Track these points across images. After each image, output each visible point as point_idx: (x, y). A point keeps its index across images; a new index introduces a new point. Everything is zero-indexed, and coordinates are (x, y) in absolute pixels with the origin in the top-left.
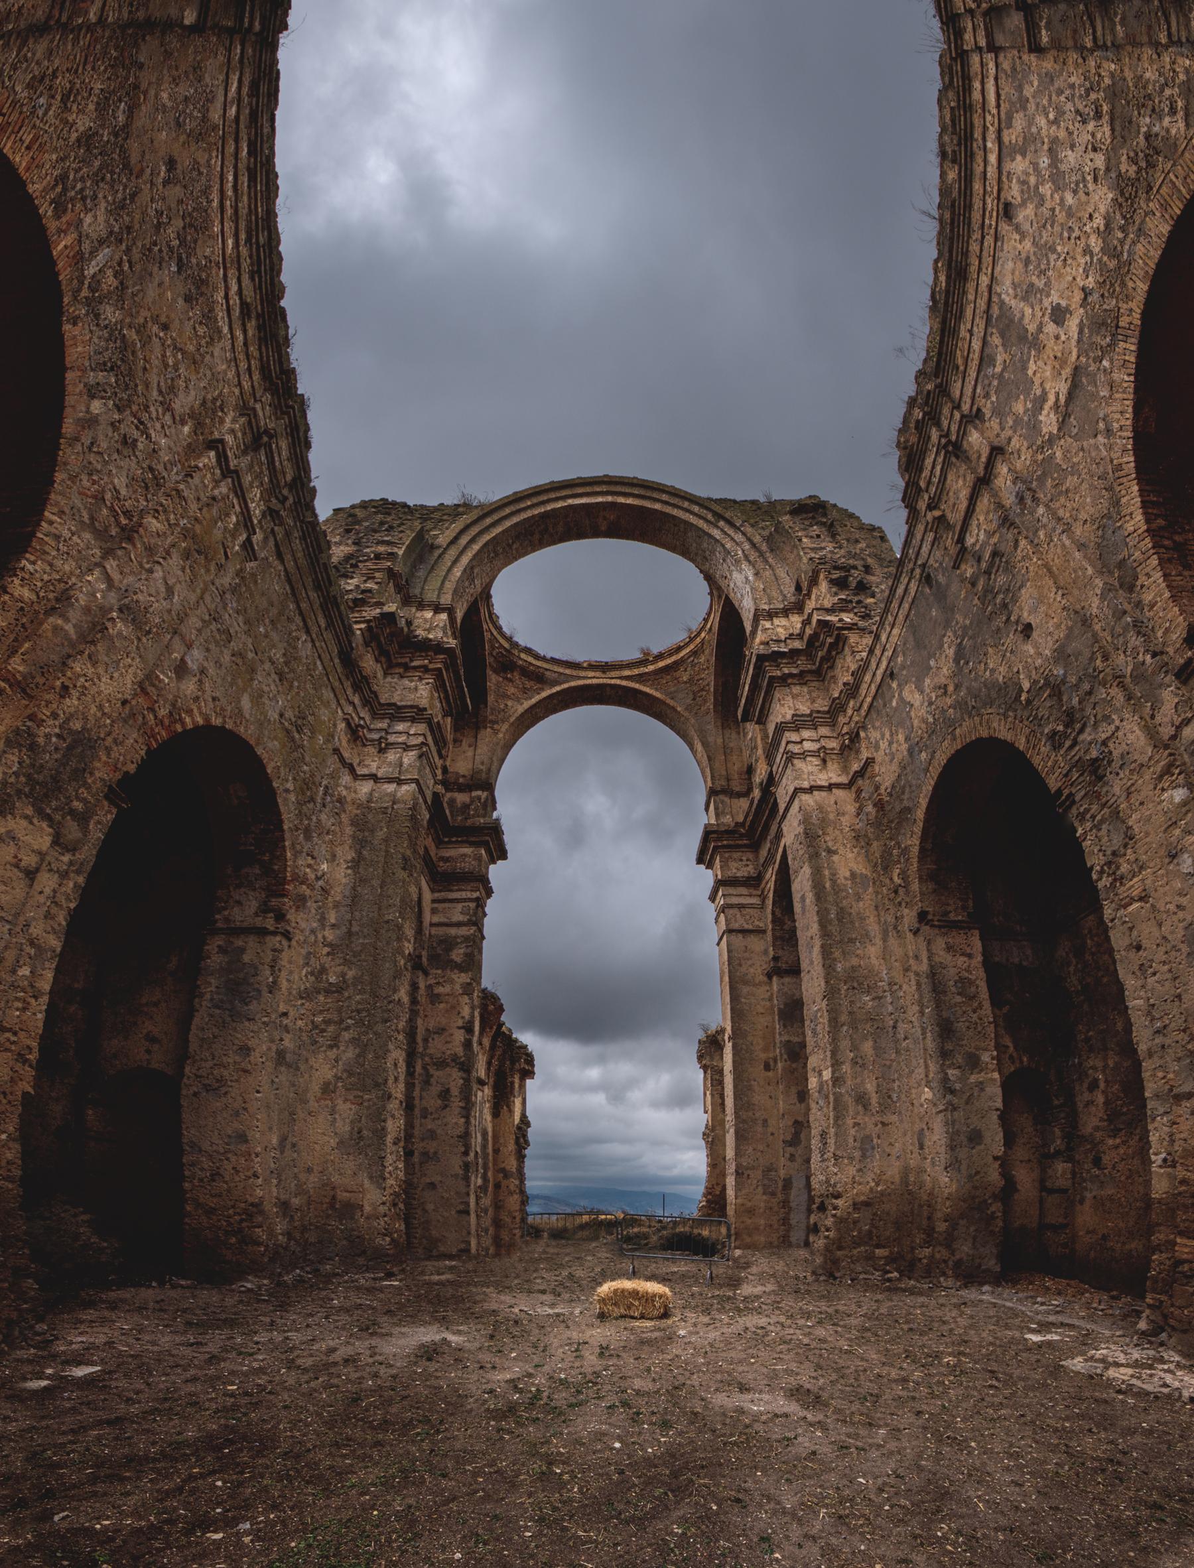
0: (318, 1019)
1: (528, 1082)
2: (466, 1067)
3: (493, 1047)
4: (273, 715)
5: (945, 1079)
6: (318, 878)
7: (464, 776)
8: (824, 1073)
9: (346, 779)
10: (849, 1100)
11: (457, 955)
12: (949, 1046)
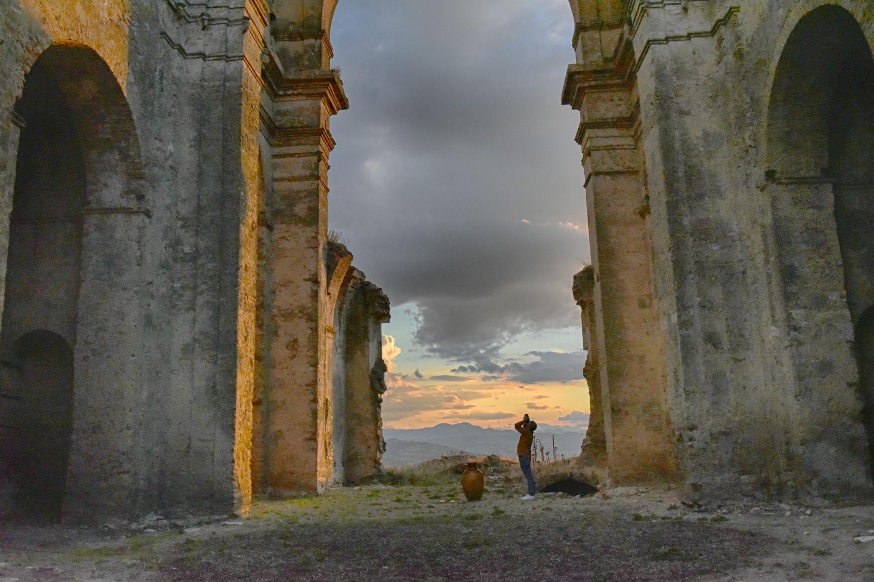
0: (177, 285)
2: (313, 318)
3: (343, 292)
4: (105, 15)
5: (789, 318)
6: (167, 159)
7: (293, 23)
8: (672, 317)
9: (177, 60)
10: (699, 341)
11: (300, 209)
12: (793, 289)
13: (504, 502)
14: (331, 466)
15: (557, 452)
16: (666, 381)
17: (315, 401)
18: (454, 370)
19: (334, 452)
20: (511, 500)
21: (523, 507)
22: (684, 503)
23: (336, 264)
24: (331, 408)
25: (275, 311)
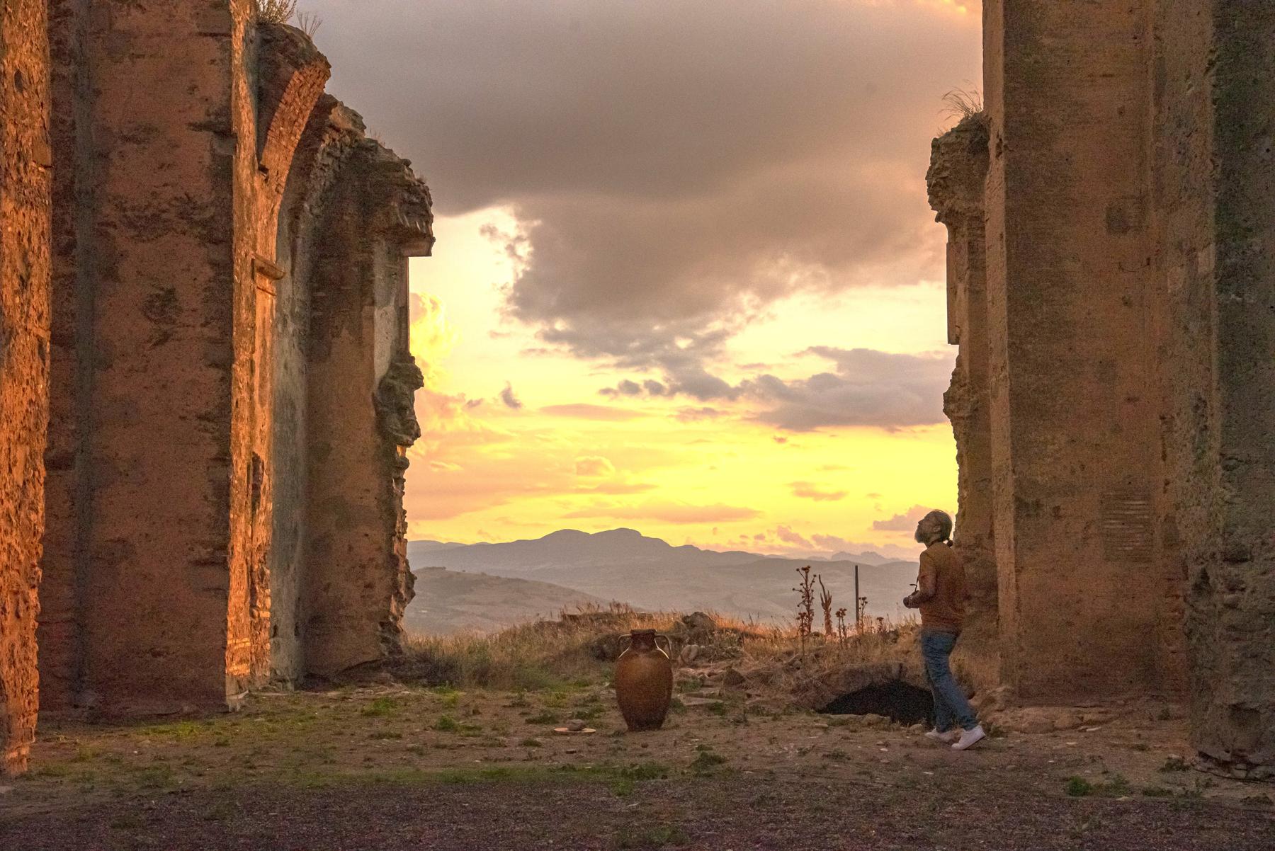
1: (414, 263)
2: (219, 235)
3: (303, 166)
8: (1201, 256)
13: (724, 734)
14: (265, 635)
15: (867, 611)
16: (1170, 430)
17: (224, 459)
18: (606, 391)
19: (276, 597)
20: (742, 731)
21: (770, 750)
22: (1204, 756)
23: (284, 86)
24: (266, 481)
25: (108, 210)
